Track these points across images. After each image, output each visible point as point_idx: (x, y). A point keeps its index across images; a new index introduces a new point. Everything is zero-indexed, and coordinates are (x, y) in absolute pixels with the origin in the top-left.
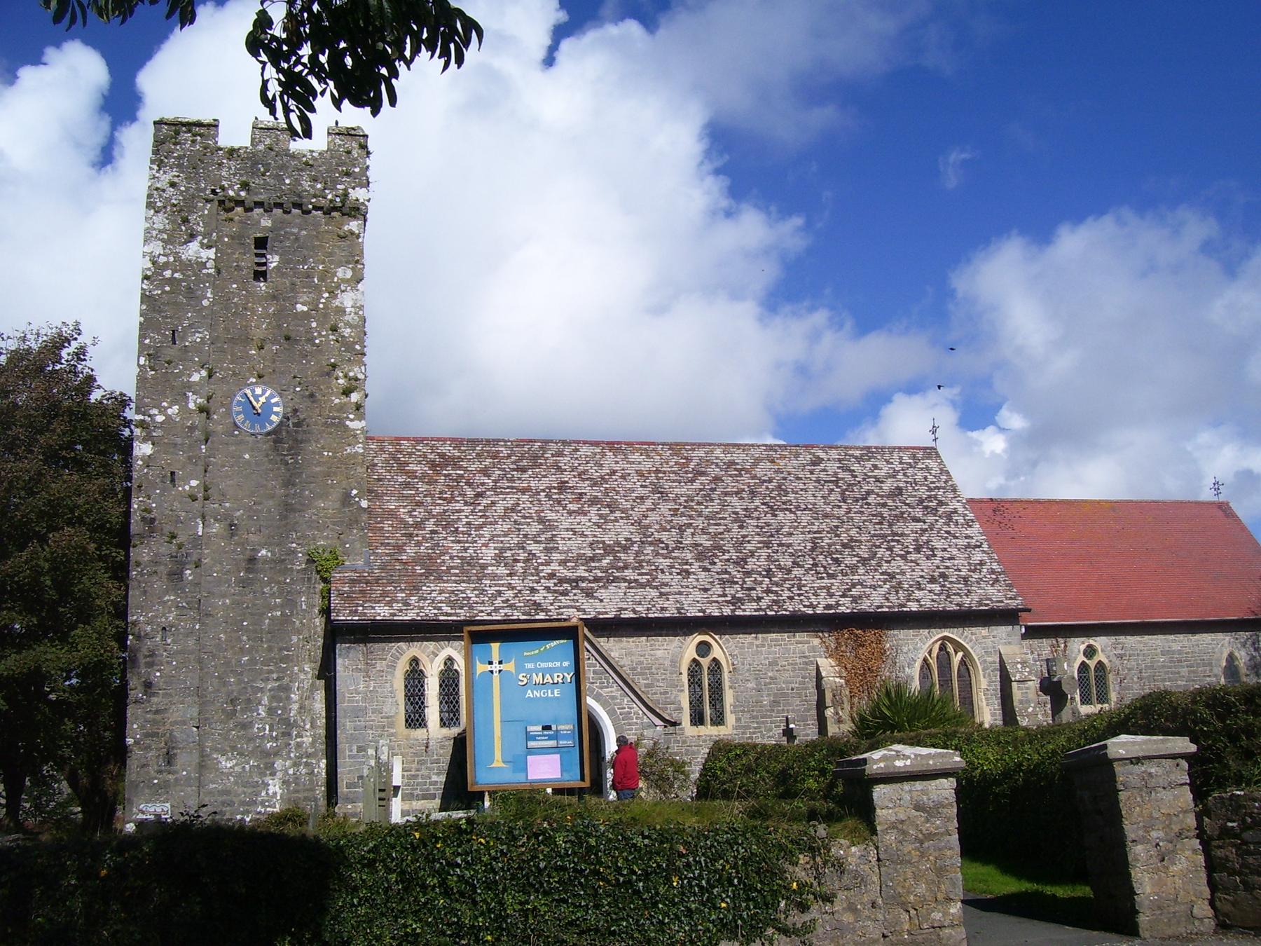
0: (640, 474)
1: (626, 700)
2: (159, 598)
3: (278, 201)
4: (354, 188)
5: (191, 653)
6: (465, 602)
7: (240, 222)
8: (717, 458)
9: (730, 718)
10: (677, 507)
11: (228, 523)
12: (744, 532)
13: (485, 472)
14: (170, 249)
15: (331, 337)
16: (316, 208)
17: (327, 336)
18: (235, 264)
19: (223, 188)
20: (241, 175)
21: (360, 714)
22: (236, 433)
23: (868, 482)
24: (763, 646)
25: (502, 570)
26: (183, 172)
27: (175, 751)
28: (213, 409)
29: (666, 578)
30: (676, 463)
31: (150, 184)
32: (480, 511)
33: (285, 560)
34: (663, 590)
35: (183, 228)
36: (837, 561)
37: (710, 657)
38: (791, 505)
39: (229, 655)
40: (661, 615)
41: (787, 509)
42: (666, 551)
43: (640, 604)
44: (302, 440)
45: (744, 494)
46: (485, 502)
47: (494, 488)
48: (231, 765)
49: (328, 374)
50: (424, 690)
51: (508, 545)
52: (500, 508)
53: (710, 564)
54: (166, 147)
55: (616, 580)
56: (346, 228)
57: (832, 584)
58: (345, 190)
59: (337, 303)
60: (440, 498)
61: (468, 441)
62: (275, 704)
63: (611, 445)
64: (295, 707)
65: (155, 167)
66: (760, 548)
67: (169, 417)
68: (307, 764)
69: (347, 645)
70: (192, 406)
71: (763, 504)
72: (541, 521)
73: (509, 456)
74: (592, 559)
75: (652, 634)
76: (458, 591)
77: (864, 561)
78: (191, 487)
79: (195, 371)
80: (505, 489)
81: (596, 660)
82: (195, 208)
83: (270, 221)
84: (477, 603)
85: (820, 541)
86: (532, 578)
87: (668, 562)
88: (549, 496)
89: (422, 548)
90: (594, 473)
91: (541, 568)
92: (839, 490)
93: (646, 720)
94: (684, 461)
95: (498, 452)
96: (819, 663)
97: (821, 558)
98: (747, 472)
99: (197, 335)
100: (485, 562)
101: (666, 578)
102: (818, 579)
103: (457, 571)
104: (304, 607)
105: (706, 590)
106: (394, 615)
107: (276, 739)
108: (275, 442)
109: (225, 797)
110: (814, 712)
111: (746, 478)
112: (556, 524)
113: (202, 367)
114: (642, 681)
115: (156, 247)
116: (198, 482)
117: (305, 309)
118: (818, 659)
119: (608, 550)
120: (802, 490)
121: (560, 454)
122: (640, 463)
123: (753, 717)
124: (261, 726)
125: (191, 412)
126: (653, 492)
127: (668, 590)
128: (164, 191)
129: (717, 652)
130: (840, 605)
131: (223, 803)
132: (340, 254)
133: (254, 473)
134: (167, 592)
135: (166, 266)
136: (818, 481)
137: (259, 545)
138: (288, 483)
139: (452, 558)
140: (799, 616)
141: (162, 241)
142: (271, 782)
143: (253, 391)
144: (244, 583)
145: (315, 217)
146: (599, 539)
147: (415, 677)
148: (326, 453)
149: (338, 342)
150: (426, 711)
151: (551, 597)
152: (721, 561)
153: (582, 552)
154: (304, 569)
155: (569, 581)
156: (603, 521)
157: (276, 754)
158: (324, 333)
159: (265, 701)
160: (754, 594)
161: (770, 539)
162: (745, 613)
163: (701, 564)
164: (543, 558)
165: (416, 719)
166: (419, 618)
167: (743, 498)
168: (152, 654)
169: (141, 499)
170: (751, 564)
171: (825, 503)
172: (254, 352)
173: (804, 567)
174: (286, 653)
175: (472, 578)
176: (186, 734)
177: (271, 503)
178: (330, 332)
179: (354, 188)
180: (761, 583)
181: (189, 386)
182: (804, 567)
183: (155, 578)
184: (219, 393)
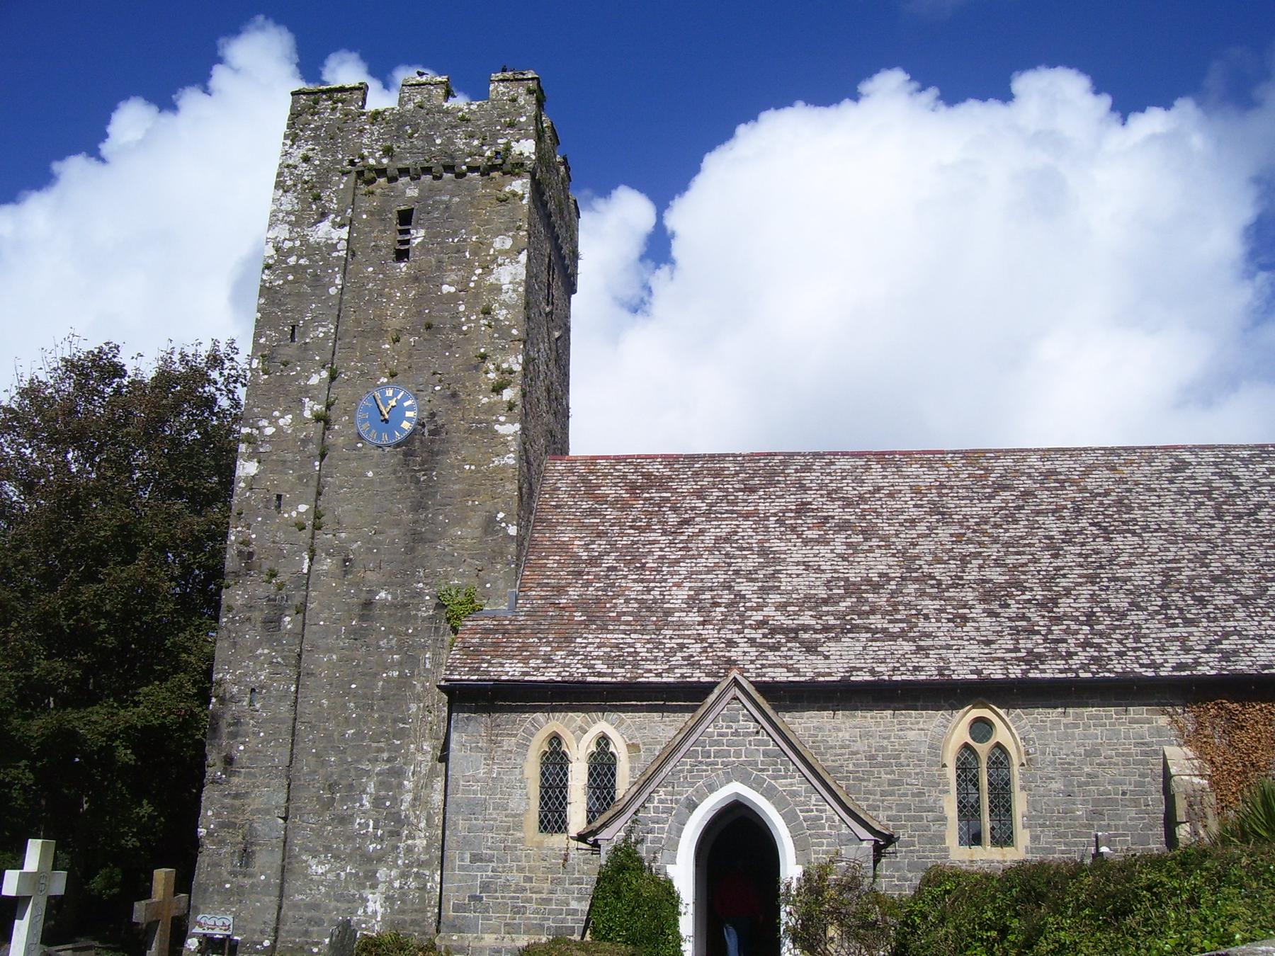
0: (916, 490)
1: (813, 798)
2: (251, 651)
3: (426, 165)
4: (518, 141)
5: (283, 722)
6: (631, 659)
7: (383, 195)
8: (1030, 467)
9: (1022, 837)
10: (964, 531)
11: (341, 557)
12: (1059, 563)
13: (700, 494)
14: (297, 232)
15: (482, 322)
16: (472, 169)
17: (478, 320)
18: (373, 244)
19: (363, 158)
20: (385, 140)
21: (478, 809)
22: (360, 445)
23: (1260, 492)
24: (1076, 726)
25: (694, 617)
26: (318, 144)
27: (254, 848)
28: (333, 418)
29: (931, 626)
30: (970, 476)
31: (281, 161)
32: (681, 542)
33: (407, 605)
34: (922, 643)
35: (314, 207)
36: (1201, 601)
37: (992, 742)
38: (1135, 525)
39: (331, 726)
40: (911, 678)
41: (1128, 531)
42: (936, 590)
43: (883, 661)
44: (438, 451)
45: (1066, 513)
46: (690, 530)
47: (707, 514)
48: (323, 871)
49: (476, 368)
50: (567, 780)
51: (710, 585)
52: (709, 539)
53: (1001, 606)
54: (302, 119)
55: (854, 629)
56: (507, 189)
57: (1191, 634)
58: (508, 144)
59: (492, 279)
60: (631, 527)
61: (687, 457)
62: (383, 793)
63: (881, 456)
64: (408, 797)
65: (289, 142)
66: (1080, 584)
67: (280, 430)
68: (418, 875)
69: (466, 715)
70: (307, 414)
71: (1091, 525)
72: (763, 552)
73: (737, 474)
74: (825, 602)
75: (902, 705)
76: (625, 643)
77: (1245, 601)
78: (298, 513)
79: (315, 373)
80: (721, 513)
81: (769, 735)
82: (330, 183)
83: (417, 191)
84: (647, 660)
85: (1175, 573)
86: (732, 627)
87: (937, 604)
88: (780, 522)
89: (590, 589)
90: (850, 491)
91: (749, 613)
92: (1213, 503)
93: (845, 830)
94: (982, 472)
95: (723, 469)
96: (1166, 753)
97: (1176, 596)
98: (1073, 483)
99: (320, 329)
100: (672, 606)
101: (931, 626)
102: (1169, 626)
103: (631, 618)
104: (428, 666)
105: (988, 643)
106: (527, 674)
107: (382, 839)
108: (405, 454)
109: (313, 913)
110: (1160, 830)
111: (1071, 491)
112: (783, 556)
113: (323, 367)
114: (883, 776)
115: (282, 232)
116: (307, 507)
117: (453, 289)
118: (1166, 748)
119: (851, 588)
120: (1153, 504)
121: (807, 468)
122: (917, 477)
123: (1060, 835)
124: (363, 821)
125: (306, 422)
126: (930, 513)
127: (931, 643)
128: (295, 167)
129: (1001, 734)
130: (1200, 664)
131: (310, 921)
132: (498, 221)
133: (377, 494)
134: (259, 644)
135: (291, 251)
136: (1180, 492)
137: (377, 586)
138: (418, 506)
139: (627, 601)
140: (1131, 680)
141: (289, 223)
142: (370, 896)
143: (383, 394)
144: (356, 634)
145: (470, 180)
146: (841, 575)
147: (555, 760)
148: (467, 467)
149: (490, 327)
150: (568, 810)
151: (753, 652)
152: (1018, 602)
153: (812, 592)
154: (431, 617)
155: (785, 630)
156: (851, 551)
157: (380, 860)
158: (473, 318)
159: (371, 788)
160: (1062, 648)
161: (1098, 571)
162: (1043, 675)
163: (986, 606)
164: (755, 600)
165: (553, 818)
166: (559, 679)
167: (1064, 518)
168: (237, 722)
169: (239, 529)
170: (1064, 606)
171: (1188, 522)
172: (387, 346)
173: (1146, 609)
174: (401, 725)
175: (648, 628)
176: (270, 827)
177: (396, 531)
178: (481, 316)
179: (518, 141)
180: (1076, 632)
181: (306, 391)
182: (1146, 609)
183: (247, 626)
184: (343, 398)
